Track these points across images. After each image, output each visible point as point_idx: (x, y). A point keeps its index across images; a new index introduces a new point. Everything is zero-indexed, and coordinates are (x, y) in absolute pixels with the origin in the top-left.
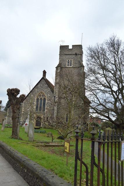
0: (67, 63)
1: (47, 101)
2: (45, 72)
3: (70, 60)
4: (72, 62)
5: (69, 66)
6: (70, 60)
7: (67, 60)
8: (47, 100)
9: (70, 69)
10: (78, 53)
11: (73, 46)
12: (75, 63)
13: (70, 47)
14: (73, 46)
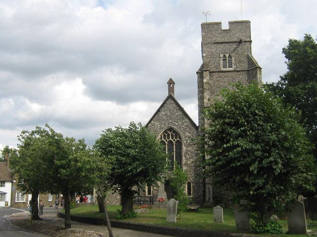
0: (222, 62)
1: (184, 148)
2: (171, 83)
3: (227, 55)
4: (233, 58)
5: (228, 69)
6: (227, 55)
7: (222, 55)
8: (185, 146)
9: (229, 74)
10: (244, 39)
11: (230, 23)
12: (240, 62)
13: (225, 26)
14: (230, 23)
